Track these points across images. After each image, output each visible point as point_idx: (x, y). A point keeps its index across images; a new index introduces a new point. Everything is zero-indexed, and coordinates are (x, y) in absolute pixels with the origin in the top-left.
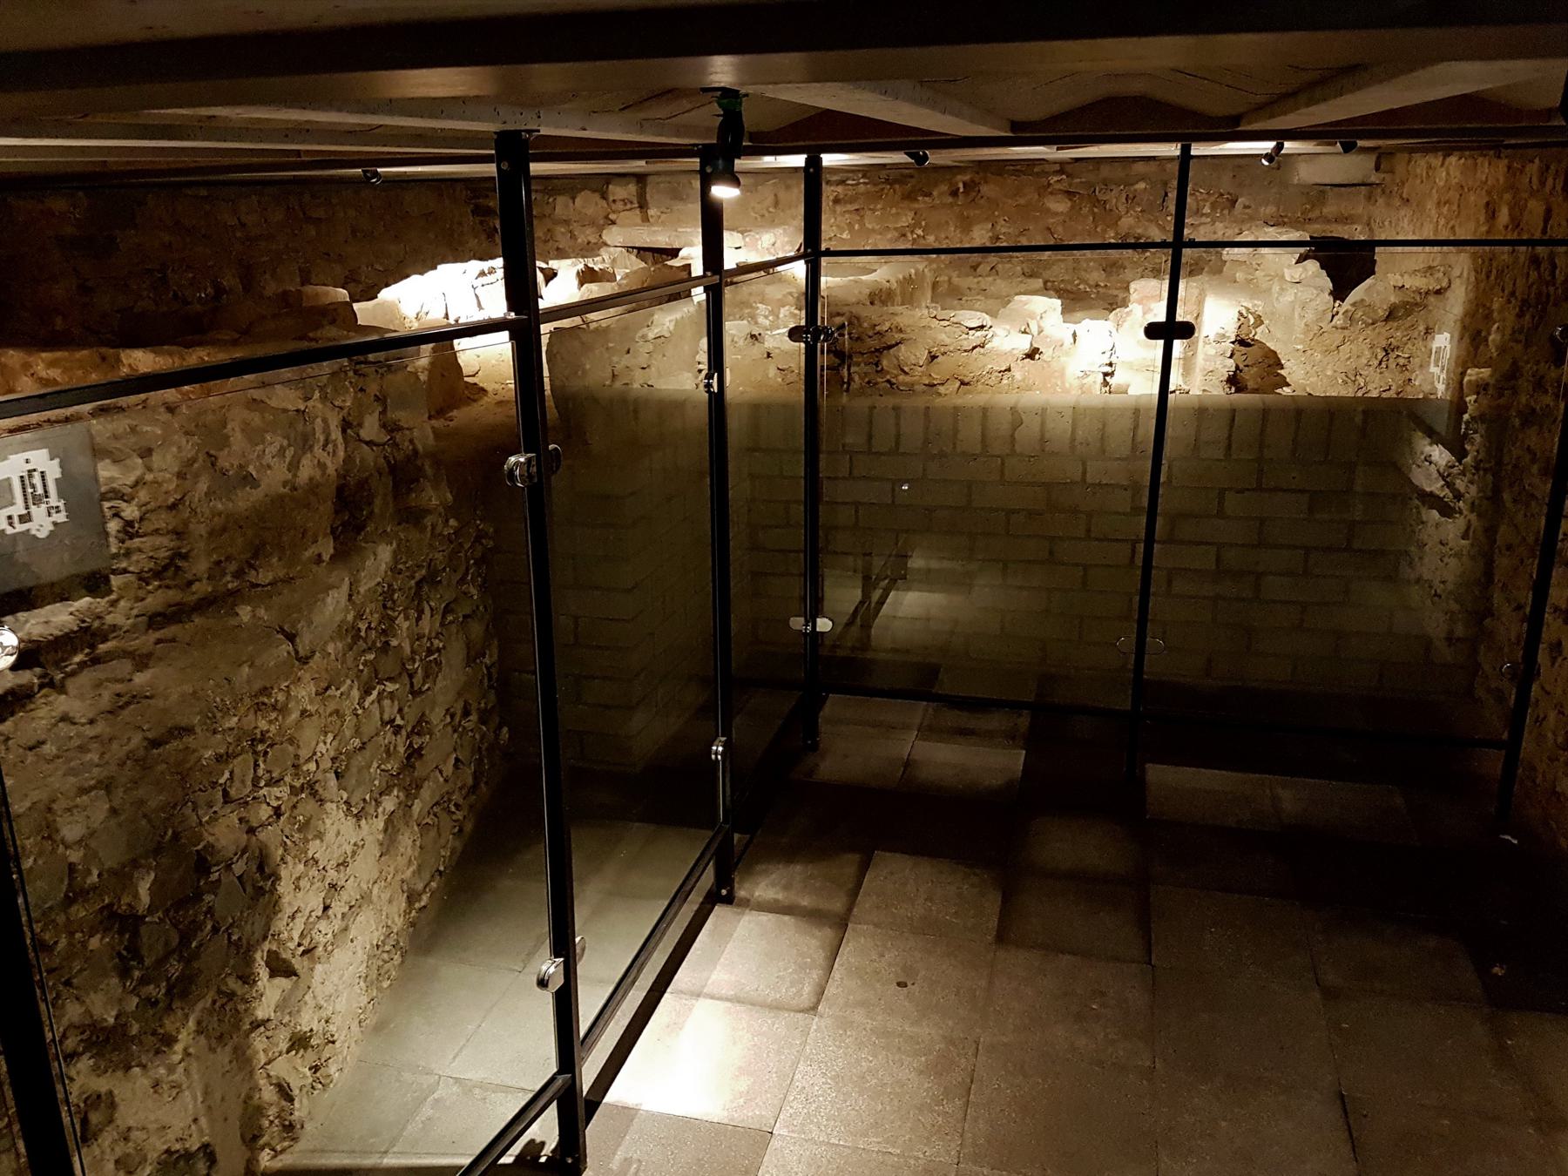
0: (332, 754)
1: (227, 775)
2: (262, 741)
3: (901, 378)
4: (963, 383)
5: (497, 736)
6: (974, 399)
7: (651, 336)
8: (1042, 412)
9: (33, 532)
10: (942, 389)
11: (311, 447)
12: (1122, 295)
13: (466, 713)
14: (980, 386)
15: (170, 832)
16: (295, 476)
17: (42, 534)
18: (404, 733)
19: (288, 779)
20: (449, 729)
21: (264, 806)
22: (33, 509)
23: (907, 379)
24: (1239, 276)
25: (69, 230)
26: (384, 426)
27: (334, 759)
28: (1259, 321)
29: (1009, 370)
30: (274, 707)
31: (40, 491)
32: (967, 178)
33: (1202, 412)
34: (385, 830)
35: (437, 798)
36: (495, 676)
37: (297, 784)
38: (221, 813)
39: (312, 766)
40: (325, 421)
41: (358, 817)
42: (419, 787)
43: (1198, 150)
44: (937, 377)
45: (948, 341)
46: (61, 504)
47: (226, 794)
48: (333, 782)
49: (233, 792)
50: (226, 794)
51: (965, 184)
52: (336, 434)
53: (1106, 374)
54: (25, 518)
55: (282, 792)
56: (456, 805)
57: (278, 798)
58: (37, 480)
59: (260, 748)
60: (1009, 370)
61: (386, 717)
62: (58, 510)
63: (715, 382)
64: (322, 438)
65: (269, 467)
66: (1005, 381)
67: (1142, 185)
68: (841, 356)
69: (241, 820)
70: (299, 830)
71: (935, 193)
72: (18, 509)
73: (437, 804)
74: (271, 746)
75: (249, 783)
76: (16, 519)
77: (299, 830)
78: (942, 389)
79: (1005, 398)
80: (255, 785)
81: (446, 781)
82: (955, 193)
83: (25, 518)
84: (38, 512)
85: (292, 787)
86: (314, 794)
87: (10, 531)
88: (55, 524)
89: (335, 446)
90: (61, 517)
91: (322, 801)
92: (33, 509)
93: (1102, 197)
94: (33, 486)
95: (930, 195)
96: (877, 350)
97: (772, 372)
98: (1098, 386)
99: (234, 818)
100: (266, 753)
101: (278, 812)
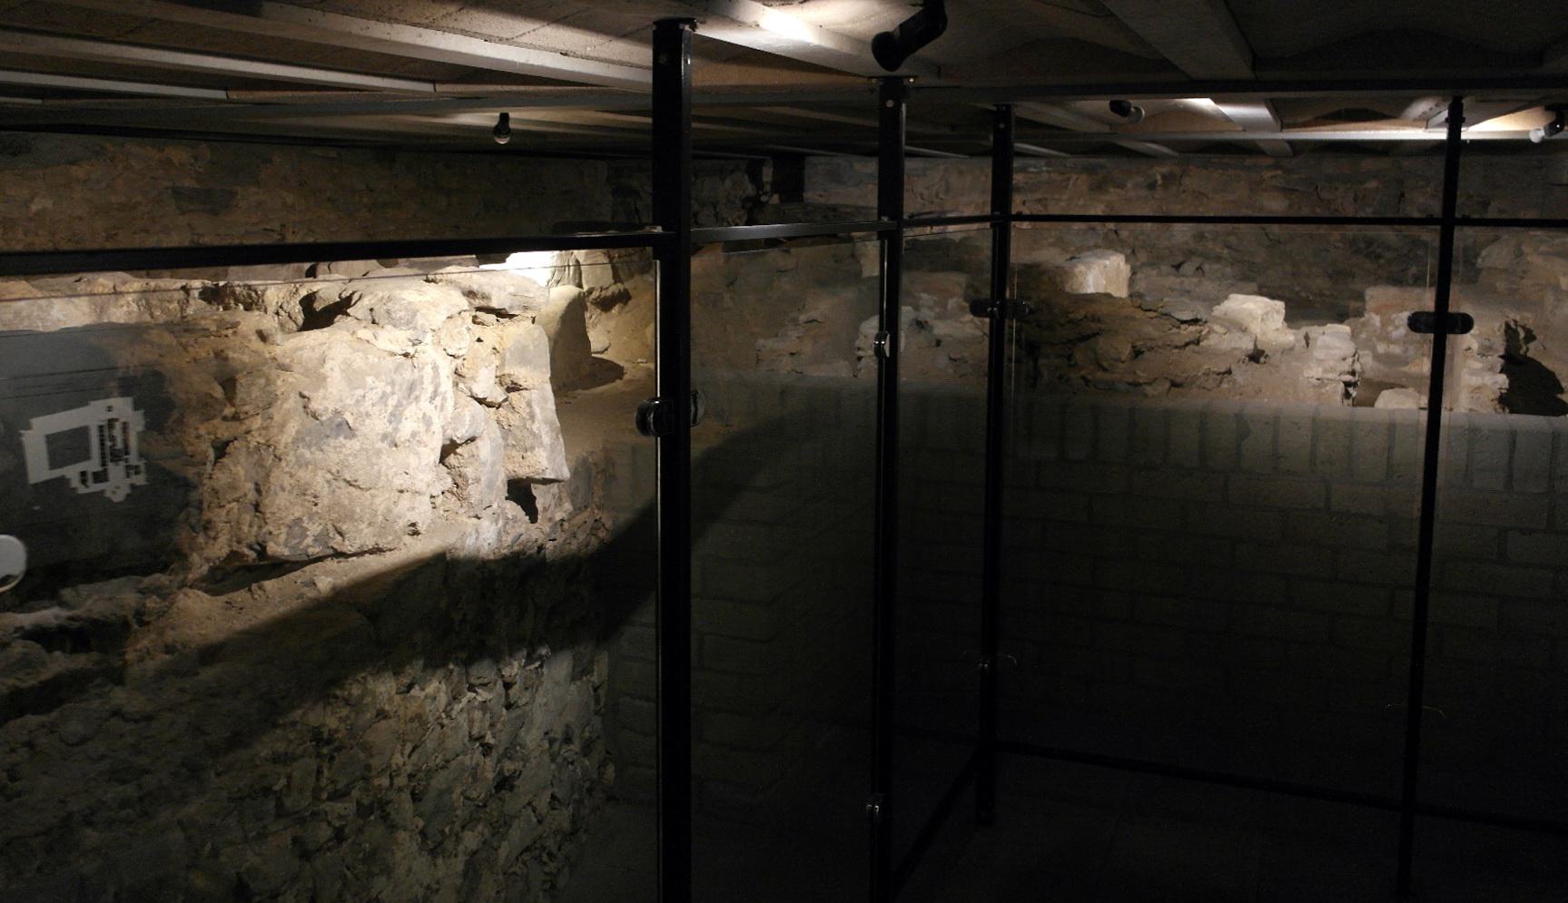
0: (409, 768)
1: (283, 781)
2: (328, 742)
3: (1100, 374)
4: (1174, 384)
5: (601, 774)
6: (1191, 401)
7: (802, 318)
8: (1275, 422)
9: (108, 494)
10: (1149, 390)
11: (417, 398)
12: (1353, 305)
13: (568, 740)
14: (1195, 391)
15: (208, 847)
16: (396, 430)
17: (119, 497)
18: (494, 754)
19: (355, 793)
20: (546, 758)
21: (324, 825)
22: (111, 466)
23: (1108, 376)
24: (1501, 285)
25: (188, 183)
26: (500, 380)
27: (411, 776)
28: (1530, 337)
29: (1229, 372)
30: (347, 702)
31: (120, 445)
32: (1165, 170)
33: (1472, 433)
34: (465, 875)
35: (528, 842)
36: (603, 700)
37: (366, 802)
38: (272, 828)
39: (385, 781)
40: (435, 368)
41: (433, 852)
42: (508, 825)
43: (1441, 134)
44: (1142, 376)
45: (1155, 334)
46: (141, 464)
47: (280, 805)
48: (408, 805)
49: (288, 802)
50: (280, 805)
51: (1164, 177)
52: (446, 384)
53: (1347, 384)
54: (100, 477)
55: (345, 808)
56: (550, 855)
57: (341, 817)
58: (117, 432)
59: (325, 751)
60: (1229, 372)
61: (475, 732)
62: (137, 470)
63: (886, 344)
64: (430, 389)
65: (368, 415)
66: (1225, 386)
67: (1372, 184)
68: (1031, 349)
69: (295, 840)
70: (364, 861)
71: (1129, 185)
72: (93, 465)
73: (527, 849)
74: (338, 749)
75: (309, 794)
76: (90, 478)
77: (364, 861)
78: (1149, 390)
79: (1227, 400)
80: (316, 793)
81: (540, 822)
82: (1152, 186)
83: (100, 477)
84: (116, 471)
85: (358, 803)
86: (385, 817)
87: (82, 490)
88: (133, 486)
89: (444, 399)
90: (140, 480)
91: (393, 827)
92: (111, 466)
93: (1324, 195)
94: (113, 439)
95: (1121, 186)
96: (1069, 341)
97: (942, 361)
98: (1339, 398)
99: (287, 838)
100: (332, 759)
101: (339, 836)
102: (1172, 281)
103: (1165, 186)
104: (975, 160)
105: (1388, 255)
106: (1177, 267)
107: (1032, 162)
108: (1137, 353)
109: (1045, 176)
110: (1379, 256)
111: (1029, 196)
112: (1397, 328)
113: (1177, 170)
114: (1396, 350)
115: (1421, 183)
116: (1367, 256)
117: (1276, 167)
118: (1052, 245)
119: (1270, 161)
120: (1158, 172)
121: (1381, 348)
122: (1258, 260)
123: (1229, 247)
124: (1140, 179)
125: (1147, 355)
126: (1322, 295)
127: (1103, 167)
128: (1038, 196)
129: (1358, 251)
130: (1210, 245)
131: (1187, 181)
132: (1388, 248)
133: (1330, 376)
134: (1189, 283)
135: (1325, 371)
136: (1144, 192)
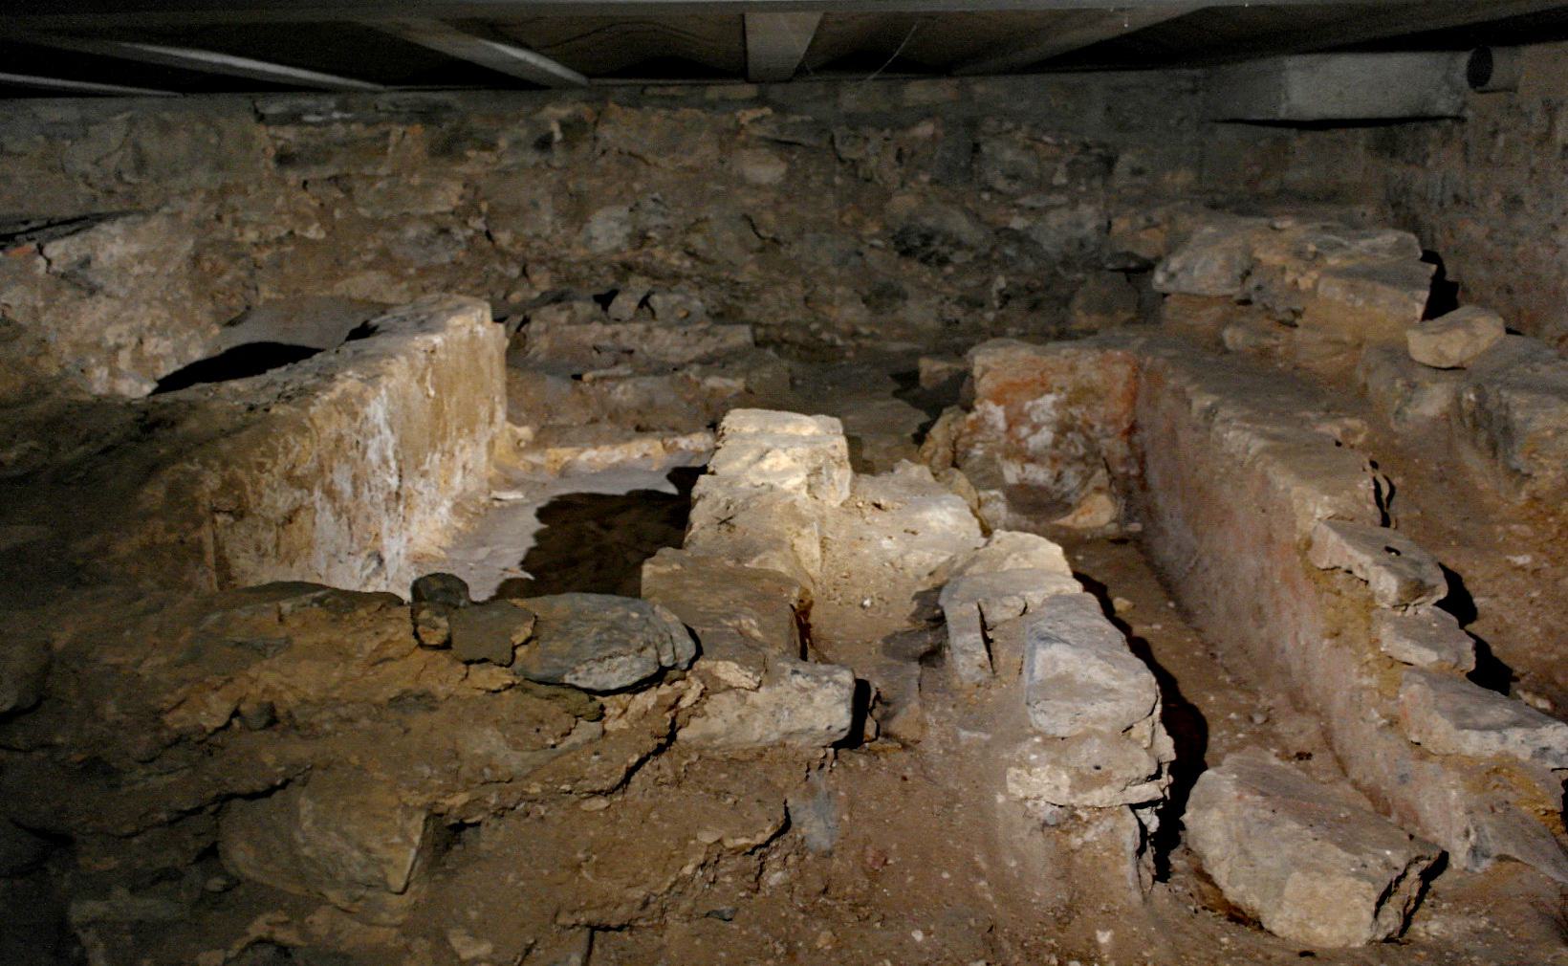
32: (564, 112)
51: (565, 126)
67: (925, 130)
82: (544, 144)
93: (848, 152)
95: (489, 146)
102: (595, 333)
103: (569, 143)
104: (190, 100)
105: (959, 258)
106: (605, 300)
107: (307, 101)
108: (447, 836)
109: (339, 131)
110: (943, 261)
111: (314, 173)
112: (1036, 428)
113: (586, 111)
114: (1040, 475)
115: (1008, 125)
116: (924, 261)
117: (760, 101)
118: (369, 266)
119: (749, 91)
120: (554, 115)
121: (1012, 473)
122: (744, 277)
123: (693, 255)
124: (520, 131)
125: (490, 838)
126: (855, 334)
127: (448, 107)
128: (331, 171)
129: (907, 253)
130: (659, 252)
131: (606, 133)
132: (959, 245)
133: (1098, 796)
134: (630, 334)
135: (1084, 781)
136: (532, 157)
